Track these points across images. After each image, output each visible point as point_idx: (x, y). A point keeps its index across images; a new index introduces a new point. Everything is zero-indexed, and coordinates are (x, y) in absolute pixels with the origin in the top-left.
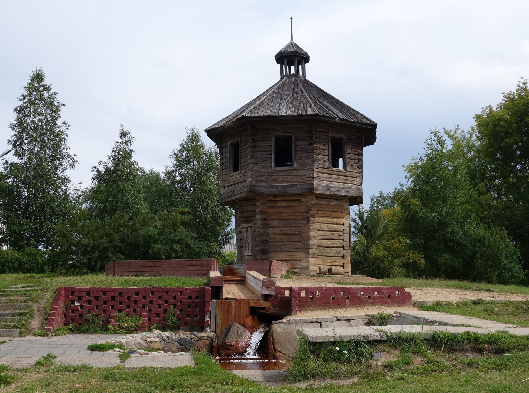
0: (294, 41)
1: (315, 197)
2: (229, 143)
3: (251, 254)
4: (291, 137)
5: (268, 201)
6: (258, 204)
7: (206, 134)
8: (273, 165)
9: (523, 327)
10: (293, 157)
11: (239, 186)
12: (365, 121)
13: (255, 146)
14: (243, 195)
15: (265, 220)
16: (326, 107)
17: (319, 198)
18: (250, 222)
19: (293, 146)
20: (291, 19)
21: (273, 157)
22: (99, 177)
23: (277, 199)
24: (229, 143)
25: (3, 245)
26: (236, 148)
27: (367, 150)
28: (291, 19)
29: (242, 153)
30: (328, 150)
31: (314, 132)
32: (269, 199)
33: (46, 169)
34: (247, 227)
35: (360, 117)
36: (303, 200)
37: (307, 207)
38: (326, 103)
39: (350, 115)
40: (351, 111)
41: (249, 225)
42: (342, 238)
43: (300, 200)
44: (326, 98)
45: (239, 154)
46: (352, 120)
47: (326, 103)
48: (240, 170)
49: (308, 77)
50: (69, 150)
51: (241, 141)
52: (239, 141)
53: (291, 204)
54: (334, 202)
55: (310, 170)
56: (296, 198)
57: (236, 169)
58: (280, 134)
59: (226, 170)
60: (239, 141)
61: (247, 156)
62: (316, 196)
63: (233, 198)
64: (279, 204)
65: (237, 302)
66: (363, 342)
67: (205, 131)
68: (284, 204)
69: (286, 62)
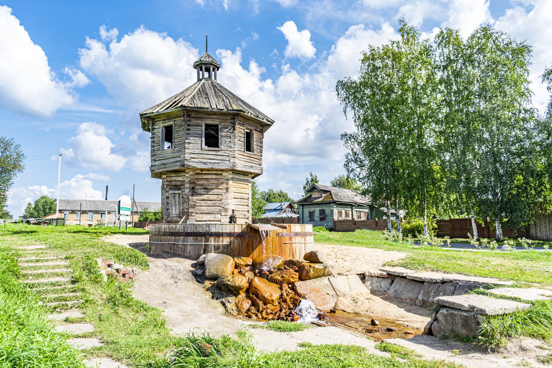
2: (161, 125)
4: (217, 126)
5: (196, 174)
9: (487, 284)
13: (189, 130)
15: (193, 188)
18: (179, 189)
29: (176, 135)
30: (244, 138)
32: (197, 172)
33: (485, 165)
41: (177, 192)
43: (221, 174)
45: (173, 135)
51: (175, 124)
53: (218, 177)
58: (209, 122)
59: (158, 147)
65: (533, 231)
66: (186, 298)
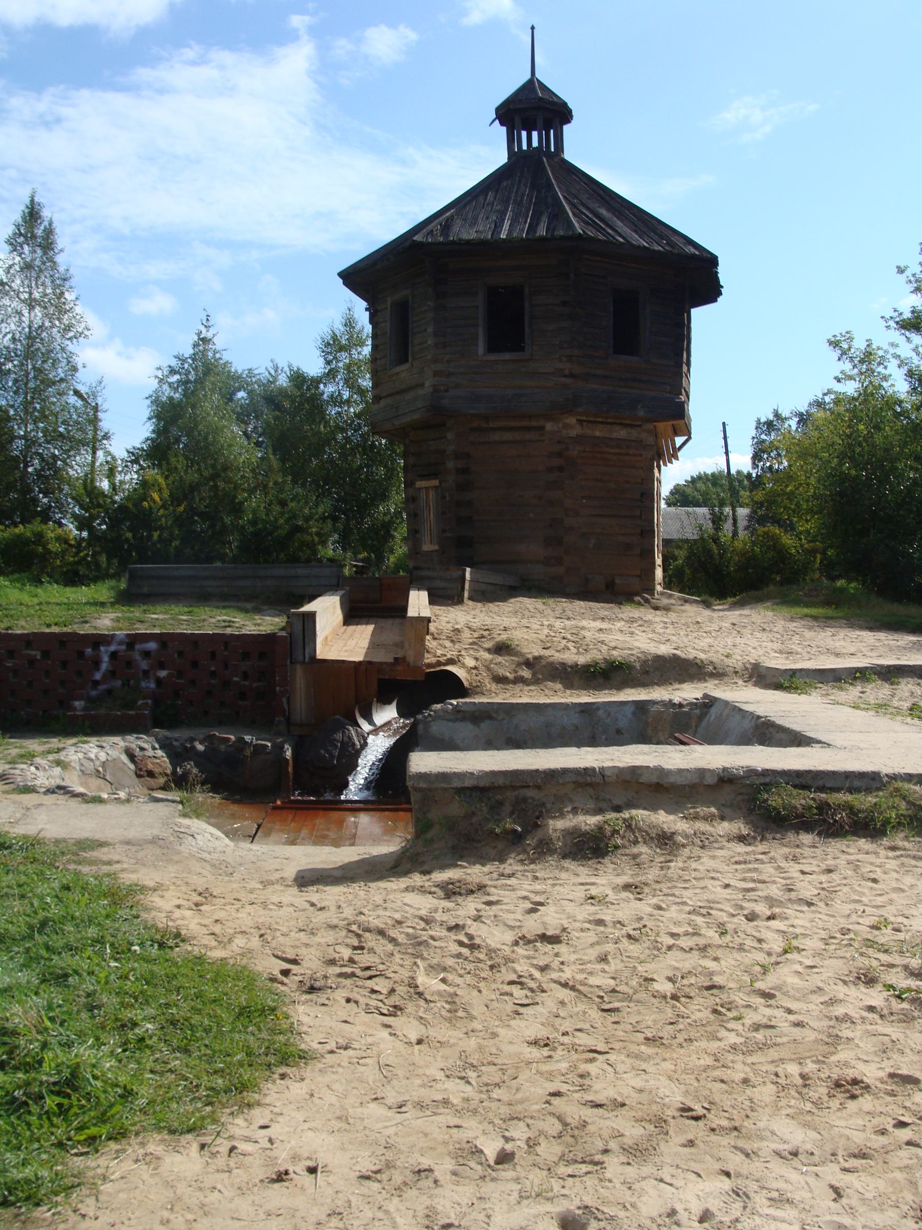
0: (538, 75)
1: (577, 420)
3: (436, 547)
6: (450, 436)
7: (341, 281)
8: (481, 349)
10: (527, 330)
11: (409, 396)
12: (691, 250)
14: (416, 416)
16: (602, 220)
17: (585, 424)
19: (527, 305)
20: (533, 28)
21: (481, 331)
22: (763, 770)
23: (491, 425)
24: (389, 301)
25: (793, 423)
26: (402, 313)
27: (700, 316)
28: (533, 28)
31: (572, 276)
34: (427, 488)
35: (679, 242)
36: (549, 426)
37: (559, 442)
38: (603, 212)
39: (655, 237)
40: (663, 229)
42: (638, 513)
43: (542, 428)
44: (606, 201)
46: (660, 248)
47: (603, 212)
48: (410, 359)
49: (571, 154)
50: (172, 365)
52: (410, 298)
54: (622, 432)
55: (564, 359)
56: (534, 423)
57: (404, 360)
60: (410, 298)
61: (425, 330)
62: (579, 418)
63: (397, 423)
64: (496, 437)
67: (342, 275)
68: (508, 436)
69: (518, 121)
